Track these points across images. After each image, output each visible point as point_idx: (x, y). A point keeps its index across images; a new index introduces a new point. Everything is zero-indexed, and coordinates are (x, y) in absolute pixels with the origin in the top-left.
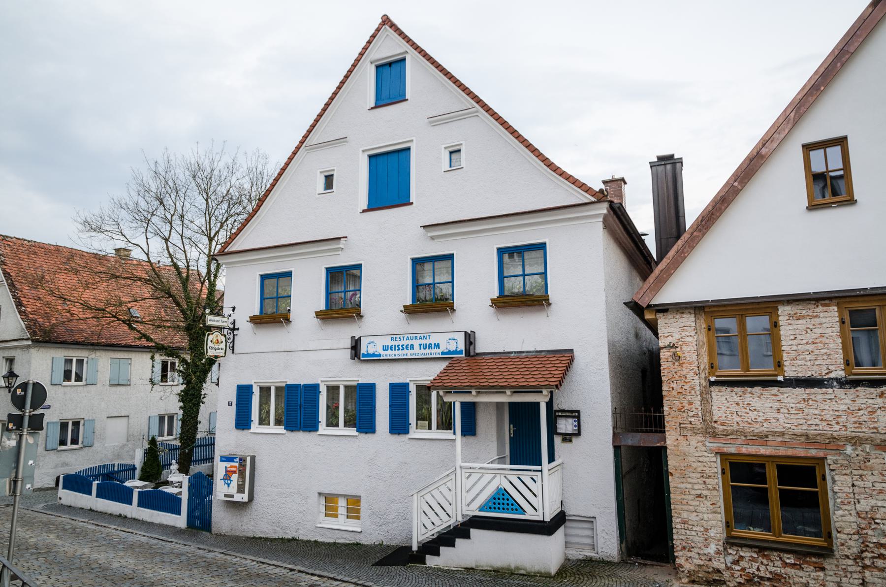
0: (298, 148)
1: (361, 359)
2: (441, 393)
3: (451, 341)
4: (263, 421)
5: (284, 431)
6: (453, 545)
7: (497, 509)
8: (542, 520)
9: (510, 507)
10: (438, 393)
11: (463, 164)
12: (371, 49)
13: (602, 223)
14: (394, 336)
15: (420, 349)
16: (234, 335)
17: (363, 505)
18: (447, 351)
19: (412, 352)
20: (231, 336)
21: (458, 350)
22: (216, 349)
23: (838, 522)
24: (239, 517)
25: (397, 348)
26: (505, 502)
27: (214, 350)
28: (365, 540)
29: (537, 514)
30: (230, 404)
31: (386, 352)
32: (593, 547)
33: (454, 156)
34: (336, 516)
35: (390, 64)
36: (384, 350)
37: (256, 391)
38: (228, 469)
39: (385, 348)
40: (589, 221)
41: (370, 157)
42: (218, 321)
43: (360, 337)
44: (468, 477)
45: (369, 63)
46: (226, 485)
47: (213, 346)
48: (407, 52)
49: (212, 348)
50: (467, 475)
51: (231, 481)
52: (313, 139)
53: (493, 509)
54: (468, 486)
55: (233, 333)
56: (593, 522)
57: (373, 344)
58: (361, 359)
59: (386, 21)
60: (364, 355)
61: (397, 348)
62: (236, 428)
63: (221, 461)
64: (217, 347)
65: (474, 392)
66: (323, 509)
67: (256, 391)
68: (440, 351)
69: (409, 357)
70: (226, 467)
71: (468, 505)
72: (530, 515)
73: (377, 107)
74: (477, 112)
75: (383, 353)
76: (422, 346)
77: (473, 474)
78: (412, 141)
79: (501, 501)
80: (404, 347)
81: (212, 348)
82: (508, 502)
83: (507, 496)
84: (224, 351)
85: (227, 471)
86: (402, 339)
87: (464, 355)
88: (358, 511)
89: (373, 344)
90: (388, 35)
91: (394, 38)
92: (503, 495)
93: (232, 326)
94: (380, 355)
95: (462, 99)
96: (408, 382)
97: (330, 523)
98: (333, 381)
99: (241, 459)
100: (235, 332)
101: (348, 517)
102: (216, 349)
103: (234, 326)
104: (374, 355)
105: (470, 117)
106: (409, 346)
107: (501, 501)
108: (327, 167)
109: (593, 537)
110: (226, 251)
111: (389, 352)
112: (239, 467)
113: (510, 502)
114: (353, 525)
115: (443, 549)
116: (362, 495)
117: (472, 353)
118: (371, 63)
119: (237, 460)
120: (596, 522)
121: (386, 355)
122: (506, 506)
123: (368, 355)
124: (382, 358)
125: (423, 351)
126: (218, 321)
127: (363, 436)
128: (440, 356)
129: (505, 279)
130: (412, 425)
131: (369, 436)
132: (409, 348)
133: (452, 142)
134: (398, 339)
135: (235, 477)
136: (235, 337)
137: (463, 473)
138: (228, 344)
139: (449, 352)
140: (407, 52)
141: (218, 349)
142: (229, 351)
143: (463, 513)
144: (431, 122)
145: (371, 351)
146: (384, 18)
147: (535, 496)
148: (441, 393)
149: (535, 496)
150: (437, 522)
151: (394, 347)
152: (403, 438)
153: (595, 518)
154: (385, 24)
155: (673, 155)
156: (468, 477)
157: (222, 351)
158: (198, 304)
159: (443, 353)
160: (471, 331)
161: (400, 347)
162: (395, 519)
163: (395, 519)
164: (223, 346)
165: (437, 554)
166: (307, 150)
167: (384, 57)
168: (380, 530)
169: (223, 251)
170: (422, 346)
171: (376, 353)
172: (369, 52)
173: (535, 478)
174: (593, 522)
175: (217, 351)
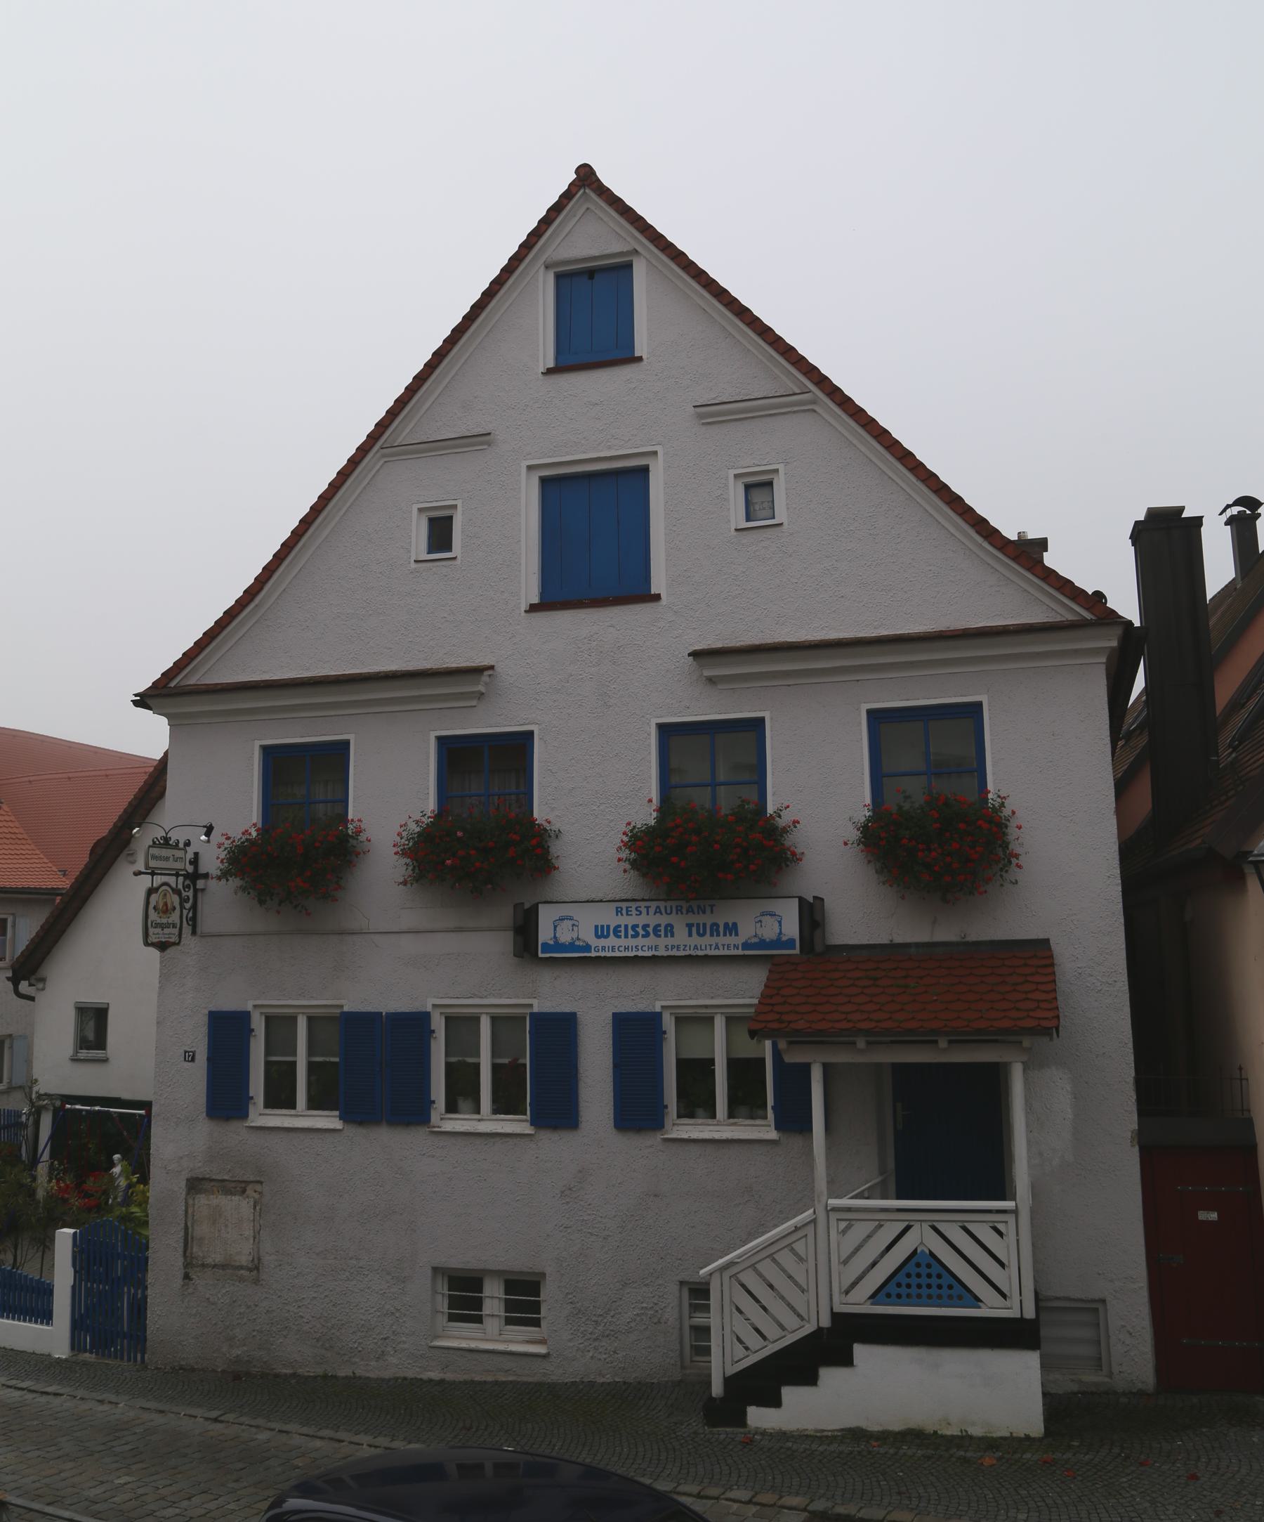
0: (363, 450)
1: (541, 955)
2: (782, 1045)
3: (767, 919)
4: (280, 1096)
5: (337, 1124)
6: (812, 1380)
7: (894, 1297)
8: (1019, 1316)
9: (945, 1291)
10: (775, 1046)
11: (781, 515)
12: (551, 235)
13: (1104, 667)
14: (624, 905)
15: (690, 935)
16: (196, 891)
17: (549, 1294)
18: (756, 940)
19: (670, 941)
20: (190, 894)
21: (784, 938)
25: (631, 932)
26: (934, 1281)
28: (556, 1373)
29: (1008, 1303)
30: (190, 1057)
31: (602, 942)
32: (1098, 1363)
33: (758, 496)
34: (479, 1319)
35: (591, 273)
36: (597, 936)
39: (601, 932)
40: (1079, 661)
41: (544, 481)
42: (167, 859)
43: (537, 905)
44: (844, 1232)
45: (543, 268)
48: (636, 252)
50: (843, 1225)
52: (403, 432)
53: (894, 1298)
54: (846, 1251)
55: (195, 885)
56: (1097, 1310)
57: (568, 923)
58: (541, 955)
59: (586, 176)
60: (546, 947)
61: (631, 932)
64: (164, 921)
65: (861, 1044)
66: (443, 1305)
68: (739, 940)
69: (662, 952)
71: (847, 1292)
72: (992, 1308)
73: (558, 369)
74: (814, 402)
75: (593, 941)
76: (694, 930)
77: (853, 1222)
78: (655, 453)
79: (924, 1281)
80: (650, 930)
82: (940, 1281)
83: (936, 1269)
84: (176, 931)
86: (644, 911)
87: (797, 951)
88: (536, 1307)
89: (571, 923)
90: (588, 209)
91: (605, 219)
92: (929, 1266)
93: (190, 869)
94: (587, 948)
95: (776, 371)
96: (658, 1009)
97: (463, 1337)
98: (463, 1002)
100: (200, 884)
101: (509, 1321)
103: (196, 868)
104: (572, 947)
105: (794, 412)
106: (662, 928)
107: (924, 1281)
108: (437, 498)
109: (1099, 1342)
110: (172, 684)
111: (612, 941)
113: (905, 1281)
114: (518, 1341)
115: (788, 1393)
116: (548, 1270)
117: (819, 948)
118: (547, 267)
120: (1106, 1310)
121: (603, 948)
122: (934, 1291)
123: (558, 946)
124: (593, 954)
125: (696, 940)
126: (167, 859)
128: (740, 952)
129: (884, 779)
130: (669, 1109)
132: (662, 933)
133: (752, 464)
134: (634, 912)
136: (199, 895)
137: (833, 1223)
138: (185, 912)
139: (763, 944)
140: (636, 252)
141: (168, 926)
142: (187, 930)
143: (835, 1310)
144: (701, 416)
145: (565, 936)
146: (582, 171)
147: (1002, 1265)
148: (782, 1045)
149: (1002, 1265)
150: (771, 1331)
151: (622, 929)
153: (1103, 1301)
154: (584, 186)
155: (1182, 509)
156: (844, 1232)
158: (412, 884)
159: (746, 946)
160: (815, 898)
161: (640, 930)
162: (633, 1324)
163: (633, 1324)
164: (175, 917)
165: (776, 1402)
166: (384, 456)
167: (579, 257)
168: (596, 1349)
169: (165, 686)
170: (694, 930)
171: (577, 943)
172: (544, 244)
173: (1001, 1227)
174: (1097, 1310)
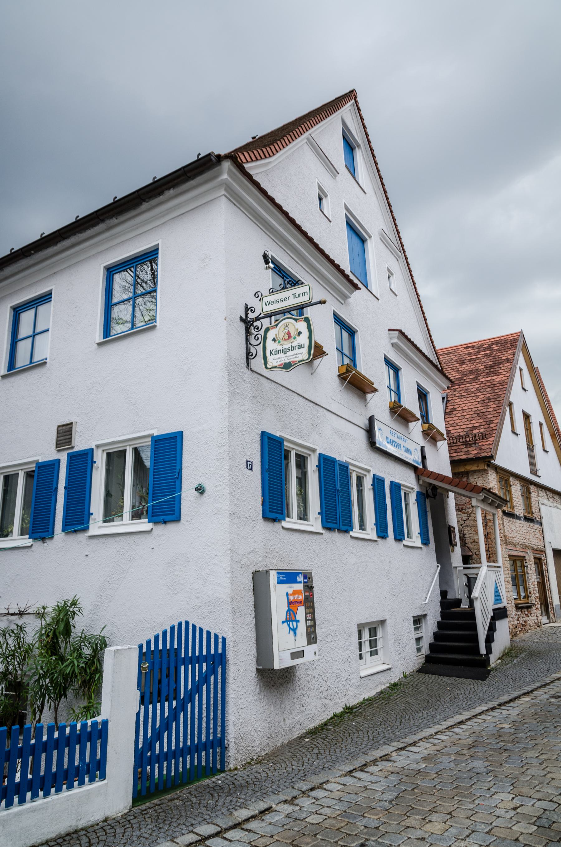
22: (285, 351)
23: (380, 826)
24: (276, 691)
27: (282, 355)
30: (250, 466)
37: (100, 459)
38: (292, 598)
46: (292, 633)
47: (280, 348)
49: (277, 352)
51: (298, 621)
62: (266, 518)
63: (280, 582)
67: (100, 459)
70: (287, 594)
81: (277, 352)
85: (290, 603)
99: (305, 577)
102: (285, 351)
112: (305, 591)
119: (300, 578)
127: (160, 529)
131: (171, 528)
135: (301, 612)
141: (292, 348)
152: (82, 537)
157: (301, 350)
175: (288, 354)
